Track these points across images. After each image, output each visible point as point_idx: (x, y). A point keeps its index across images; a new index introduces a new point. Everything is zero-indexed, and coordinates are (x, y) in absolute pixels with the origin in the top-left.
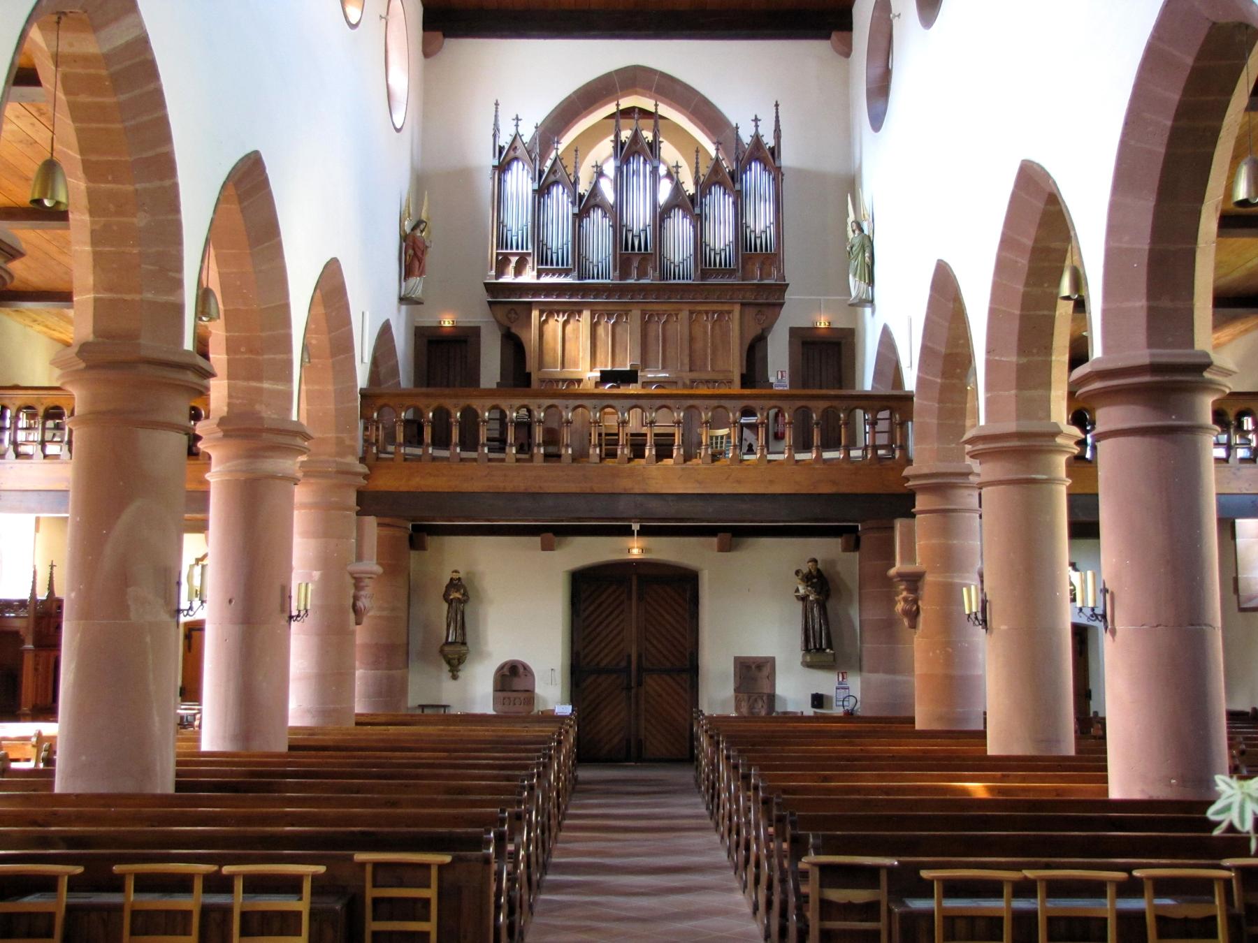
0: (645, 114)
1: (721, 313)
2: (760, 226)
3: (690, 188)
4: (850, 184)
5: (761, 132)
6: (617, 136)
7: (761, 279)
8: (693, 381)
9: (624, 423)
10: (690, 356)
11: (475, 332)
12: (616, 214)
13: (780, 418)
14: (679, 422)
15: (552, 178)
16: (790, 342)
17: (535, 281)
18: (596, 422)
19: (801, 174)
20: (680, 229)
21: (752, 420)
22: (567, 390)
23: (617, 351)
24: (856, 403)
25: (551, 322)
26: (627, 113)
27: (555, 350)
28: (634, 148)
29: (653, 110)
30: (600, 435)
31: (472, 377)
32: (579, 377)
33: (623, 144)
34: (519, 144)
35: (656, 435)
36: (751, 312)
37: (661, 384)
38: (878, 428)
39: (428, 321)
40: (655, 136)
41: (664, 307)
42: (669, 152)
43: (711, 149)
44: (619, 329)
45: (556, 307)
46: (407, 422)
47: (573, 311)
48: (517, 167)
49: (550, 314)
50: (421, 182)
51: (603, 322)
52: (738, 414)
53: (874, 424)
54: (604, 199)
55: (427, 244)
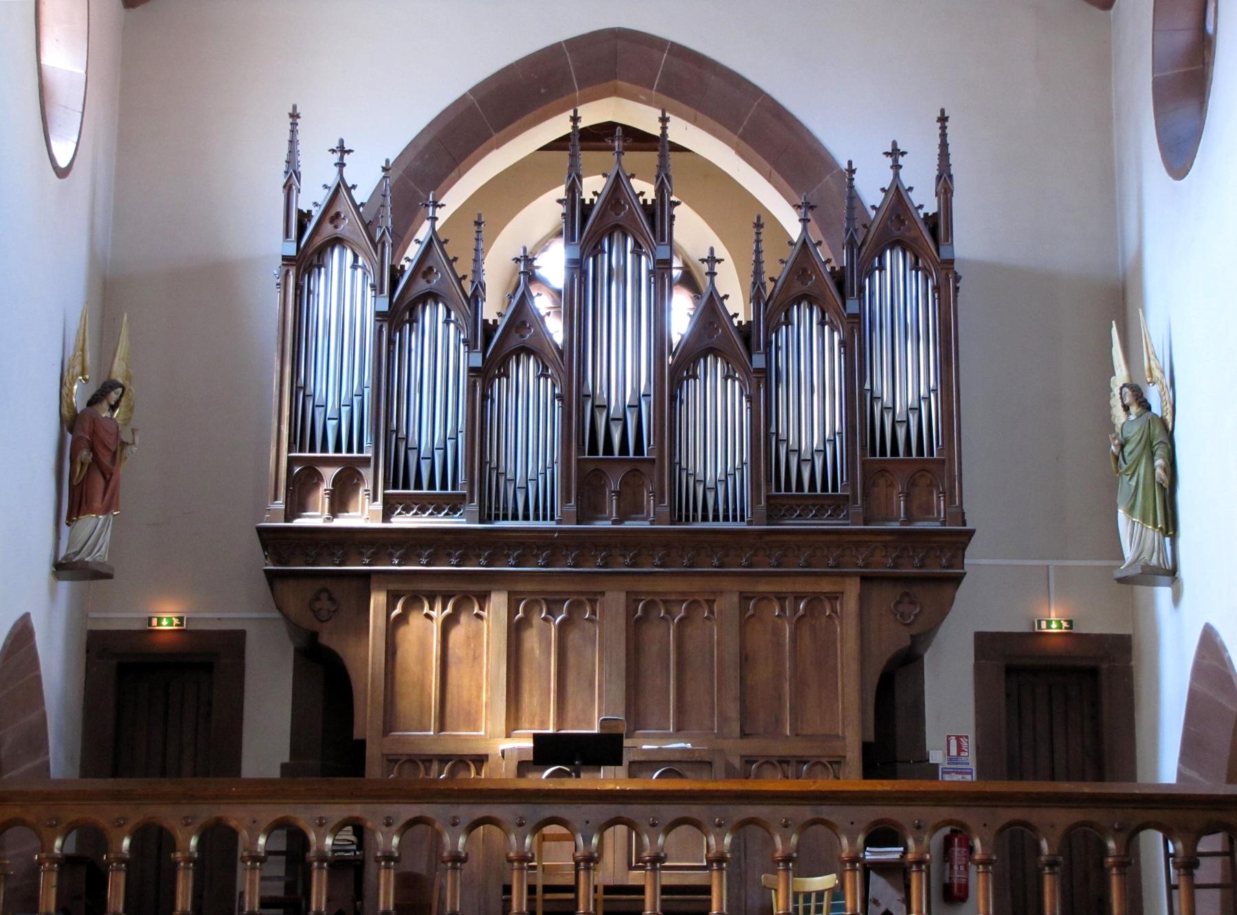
0: (637, 139)
1: (815, 600)
2: (906, 396)
3: (738, 307)
4: (1116, 300)
5: (906, 179)
6: (573, 190)
7: (909, 519)
8: (748, 761)
9: (590, 861)
10: (743, 700)
11: (233, 642)
12: (570, 367)
13: (957, 851)
14: (720, 859)
15: (422, 286)
16: (978, 669)
17: (379, 524)
18: (523, 859)
19: (1001, 275)
20: (717, 401)
21: (892, 854)
22: (452, 781)
23: (571, 689)
24: (1141, 815)
25: (416, 620)
26: (598, 137)
27: (423, 686)
28: (612, 219)
29: (657, 132)
30: (532, 889)
31: (220, 750)
32: (480, 750)
33: (586, 209)
34: (343, 206)
35: (666, 890)
36: (885, 596)
37: (672, 766)
38: (1201, 875)
39: (120, 616)
40: (660, 191)
41: (681, 585)
42: (692, 232)
43: (791, 224)
44: (574, 637)
45: (427, 586)
46: (67, 863)
47: (466, 595)
48: (339, 260)
49: (414, 601)
50: (112, 293)
51: (537, 620)
52: (860, 840)
53: (1189, 864)
54: (543, 334)
55: (126, 436)
